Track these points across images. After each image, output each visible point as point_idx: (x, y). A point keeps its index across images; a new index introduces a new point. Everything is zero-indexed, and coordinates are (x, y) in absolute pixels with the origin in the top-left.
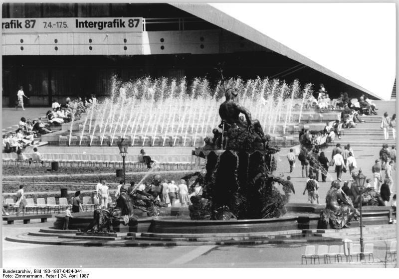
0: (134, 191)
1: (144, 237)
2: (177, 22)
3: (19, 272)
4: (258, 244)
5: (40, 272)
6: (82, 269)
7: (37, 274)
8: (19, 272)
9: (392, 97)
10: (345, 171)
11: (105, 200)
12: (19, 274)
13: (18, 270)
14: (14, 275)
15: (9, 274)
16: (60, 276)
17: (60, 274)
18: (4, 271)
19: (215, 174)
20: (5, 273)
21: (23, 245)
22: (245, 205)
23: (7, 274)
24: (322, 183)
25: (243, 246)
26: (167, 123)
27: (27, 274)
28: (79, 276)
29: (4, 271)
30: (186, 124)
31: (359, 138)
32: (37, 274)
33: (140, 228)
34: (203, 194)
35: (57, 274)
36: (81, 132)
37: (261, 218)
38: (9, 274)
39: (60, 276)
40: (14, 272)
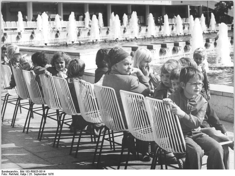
1: (106, 90)
2: (206, 12)
3: (11, 172)
4: (190, 63)
8: (11, 172)
9: (226, 168)
14: (8, 173)
15: (6, 173)
16: (29, 174)
17: (29, 173)
18: (2, 171)
19: (224, 4)
20: (3, 173)
22: (195, 14)
23: (4, 173)
24: (28, 16)
27: (15, 173)
31: (209, 55)
34: (68, 76)
36: (8, 51)
37: (107, 155)
38: (6, 173)
39: (29, 174)
40: (8, 172)
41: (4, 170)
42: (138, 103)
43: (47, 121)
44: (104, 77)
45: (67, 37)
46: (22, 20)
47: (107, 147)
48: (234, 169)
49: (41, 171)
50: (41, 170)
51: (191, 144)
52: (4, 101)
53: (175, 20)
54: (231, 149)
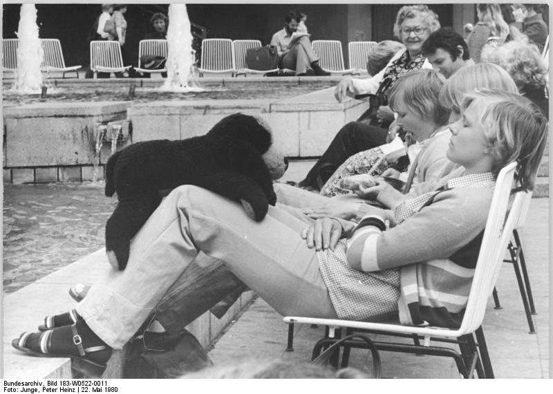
0: (393, 62)
3: (27, 384)
5: (56, 384)
6: (108, 380)
7: (52, 387)
8: (27, 384)
10: (342, 182)
11: (11, 281)
12: (26, 387)
13: (25, 381)
14: (20, 388)
15: (13, 387)
16: (81, 390)
18: (5, 383)
21: (35, 361)
23: (10, 387)
25: (450, 338)
26: (108, 23)
28: (104, 390)
29: (5, 383)
30: (113, 75)
32: (52, 387)
33: (412, 283)
35: (76, 387)
38: (13, 387)
39: (81, 390)
40: (19, 384)
41: (9, 381)
42: (411, 7)
43: (37, 172)
44: (255, 47)
45: (389, 209)
46: (37, 34)
47: (71, 80)
48: (550, 377)
49: (97, 383)
50: (97, 380)
51: (410, 263)
52: (515, 263)
53: (468, 329)
54: (84, 321)
